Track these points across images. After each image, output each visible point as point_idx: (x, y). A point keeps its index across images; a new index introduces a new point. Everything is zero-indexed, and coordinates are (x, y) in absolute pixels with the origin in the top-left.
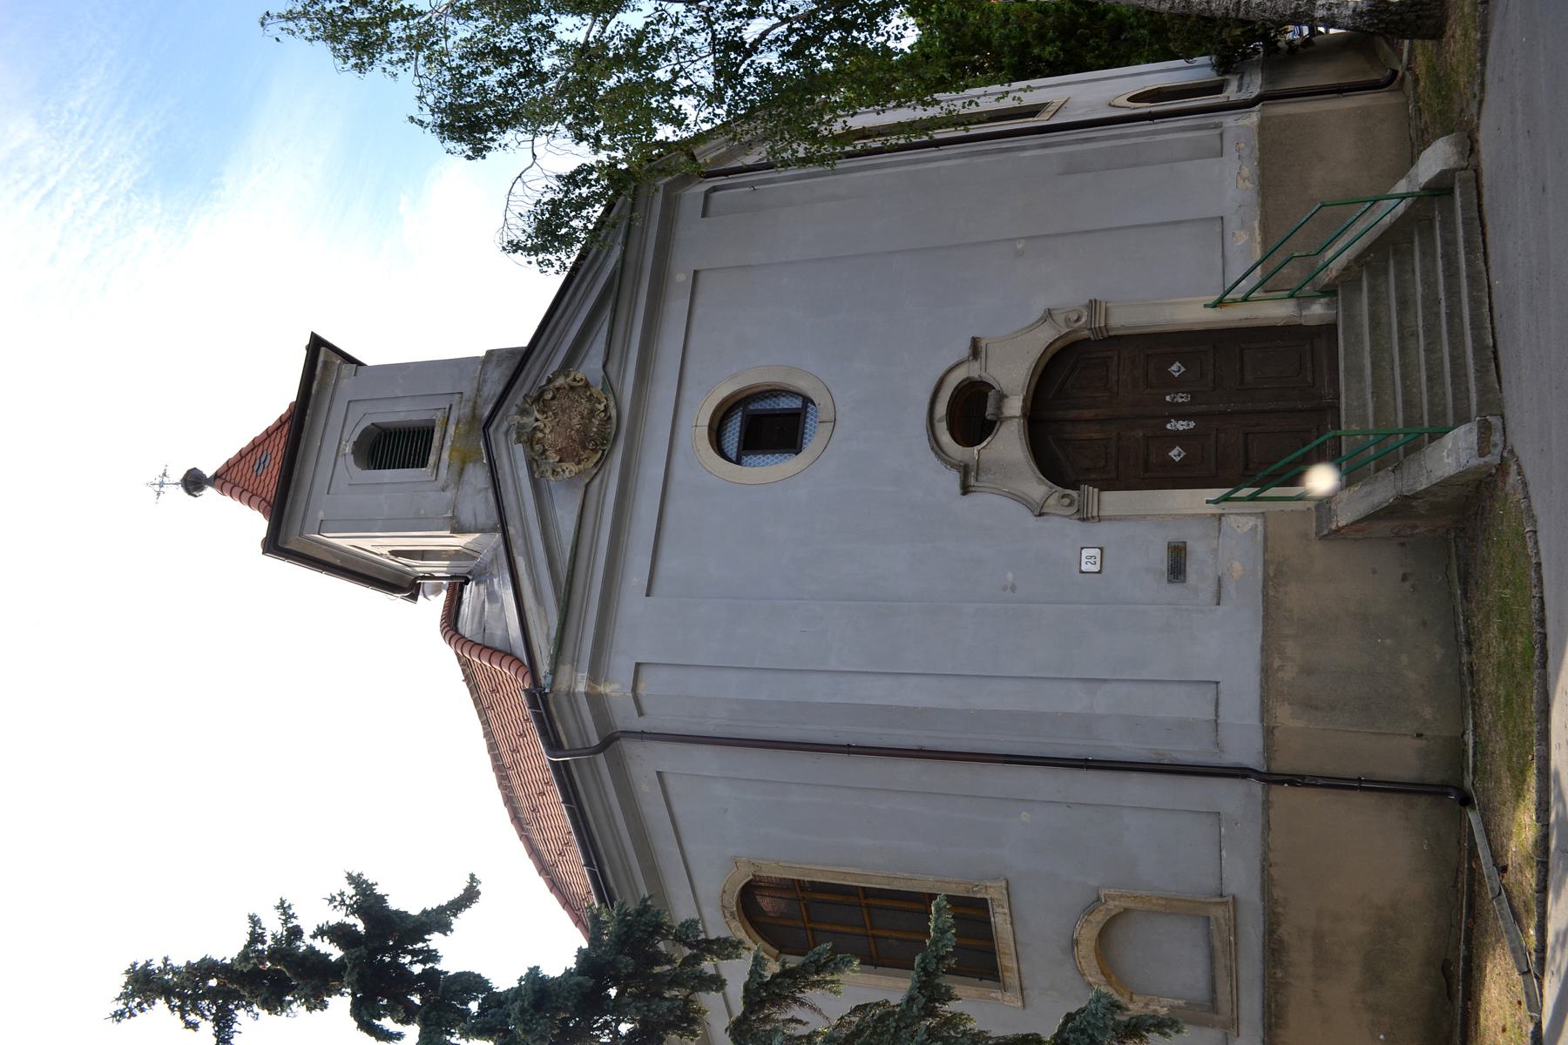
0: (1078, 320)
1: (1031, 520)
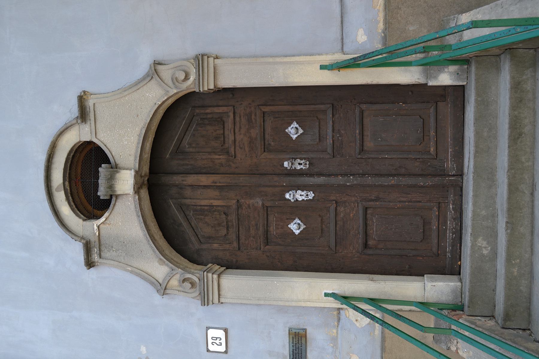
0: (187, 78)
1: (157, 298)
